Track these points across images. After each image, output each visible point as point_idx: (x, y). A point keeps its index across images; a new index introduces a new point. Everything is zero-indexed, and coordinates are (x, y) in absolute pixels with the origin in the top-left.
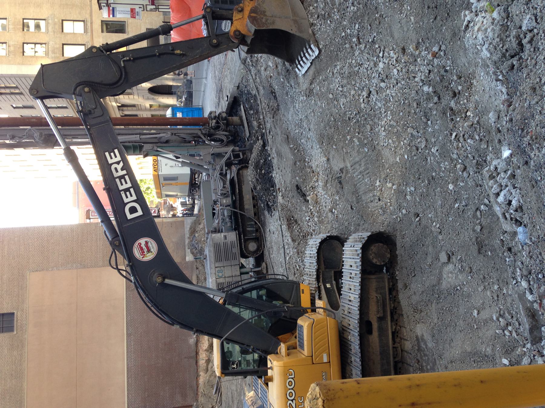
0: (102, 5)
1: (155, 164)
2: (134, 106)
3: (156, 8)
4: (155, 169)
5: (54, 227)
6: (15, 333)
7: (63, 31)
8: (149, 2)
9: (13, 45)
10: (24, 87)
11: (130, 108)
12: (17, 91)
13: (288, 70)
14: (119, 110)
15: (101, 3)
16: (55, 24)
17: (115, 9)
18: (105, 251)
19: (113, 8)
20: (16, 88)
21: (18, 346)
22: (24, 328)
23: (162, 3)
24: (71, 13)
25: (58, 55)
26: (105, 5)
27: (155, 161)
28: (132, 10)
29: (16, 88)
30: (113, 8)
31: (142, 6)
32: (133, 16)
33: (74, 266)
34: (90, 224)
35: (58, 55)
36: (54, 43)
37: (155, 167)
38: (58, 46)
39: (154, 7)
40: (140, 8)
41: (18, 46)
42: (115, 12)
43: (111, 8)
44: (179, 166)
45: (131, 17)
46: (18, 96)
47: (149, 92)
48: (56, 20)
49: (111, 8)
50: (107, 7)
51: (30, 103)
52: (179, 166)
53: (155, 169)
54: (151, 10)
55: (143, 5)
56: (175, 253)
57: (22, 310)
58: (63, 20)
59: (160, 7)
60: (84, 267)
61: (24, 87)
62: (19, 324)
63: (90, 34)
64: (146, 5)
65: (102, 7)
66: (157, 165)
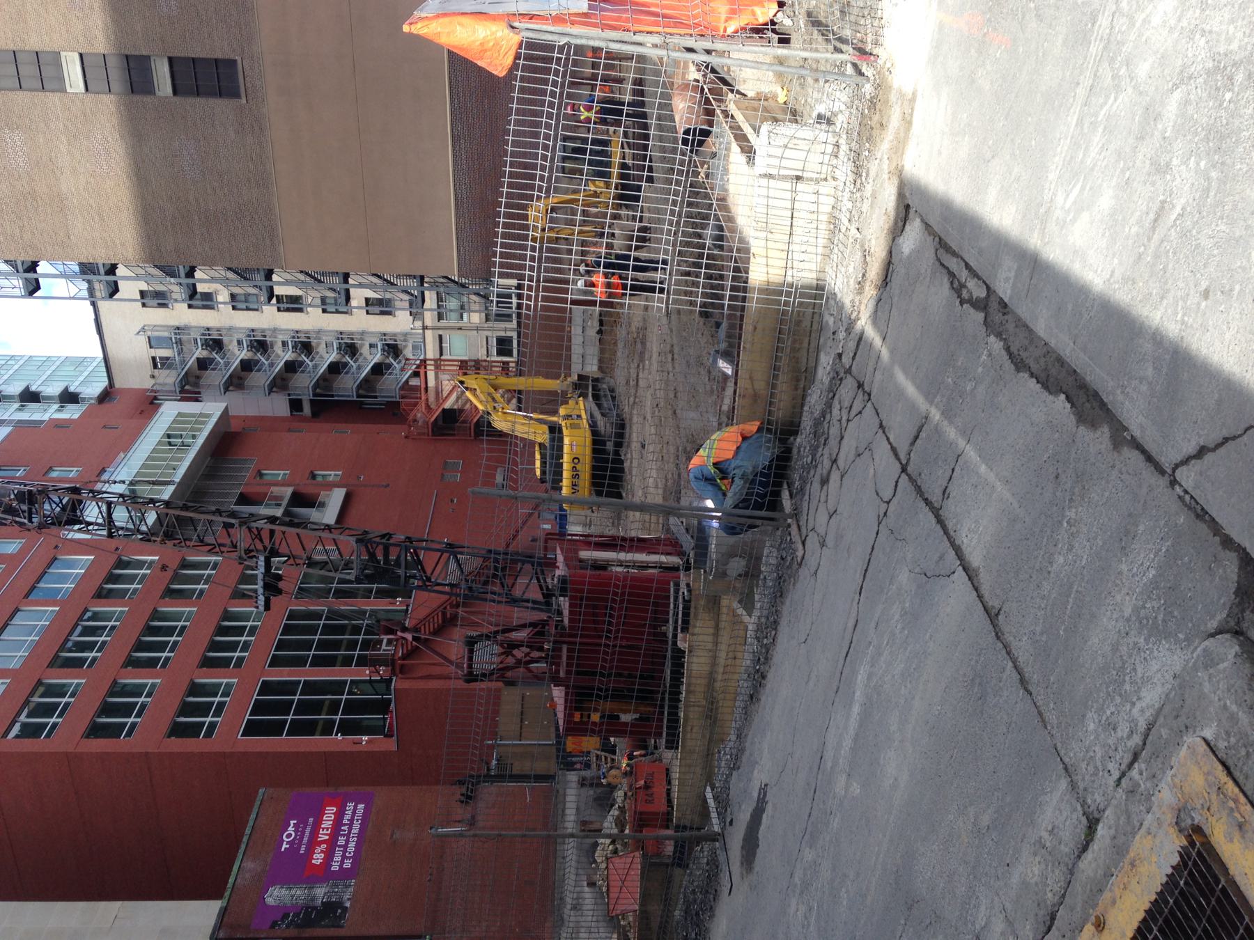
22: (259, 94)
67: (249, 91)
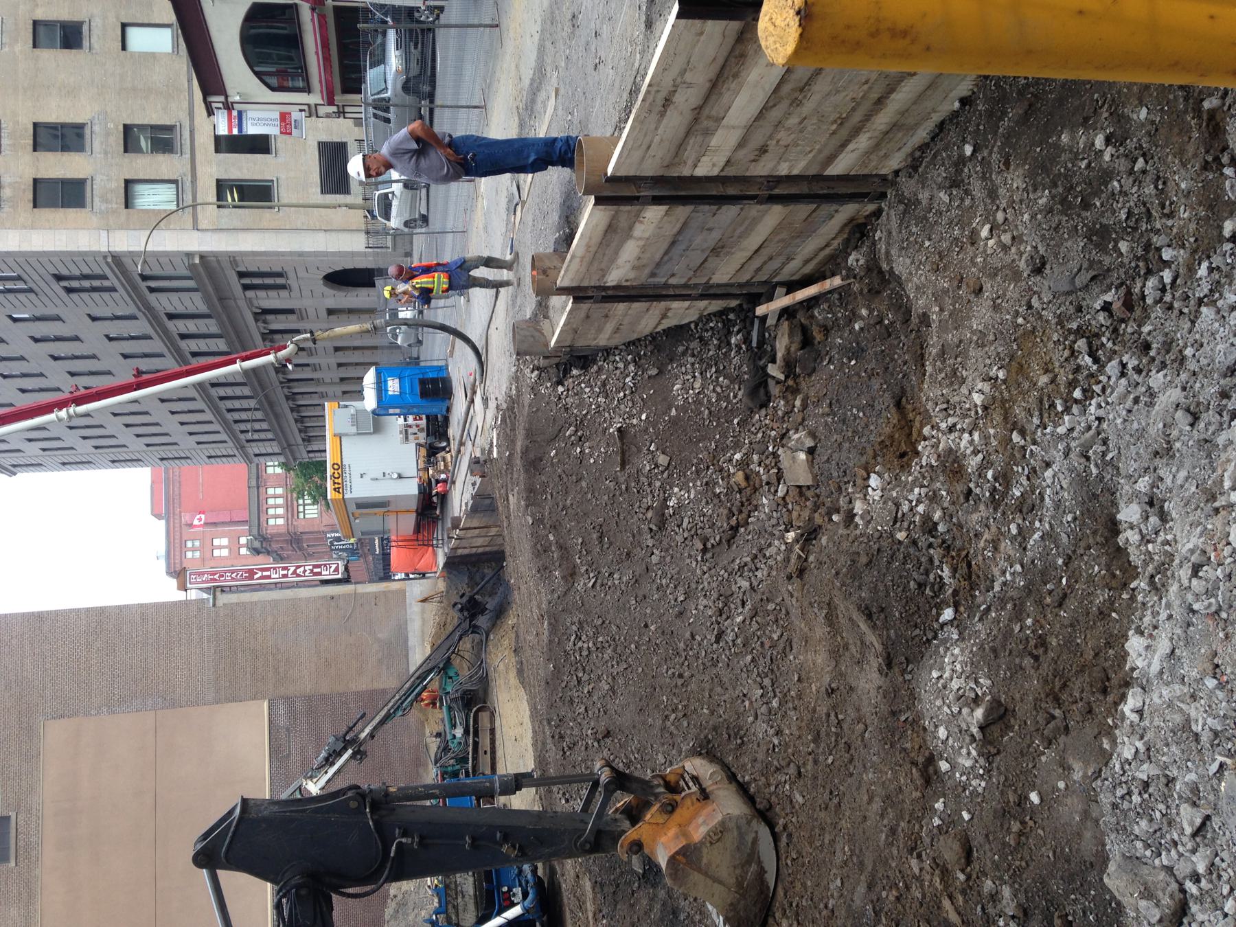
0: (214, 105)
1: (336, 475)
2: (291, 311)
3: (339, 112)
4: (337, 486)
5: (102, 611)
6: (13, 864)
7: (124, 48)
8: (323, 99)
9: (10, 184)
10: (36, 277)
11: (281, 317)
12: (20, 285)
13: (666, 100)
14: (257, 321)
15: (210, 102)
16: (108, 134)
17: (244, 115)
18: (221, 667)
19: (240, 113)
20: (19, 278)
21: (20, 894)
22: (33, 853)
23: (353, 101)
24: (144, 109)
25: (115, 206)
26: (220, 105)
27: (336, 467)
28: (284, 117)
29: (19, 278)
30: (240, 113)
31: (306, 108)
32: (286, 132)
33: (150, 702)
34: (187, 603)
35: (115, 206)
36: (105, 178)
37: (336, 481)
38: (113, 185)
39: (334, 109)
40: (301, 111)
41: (23, 187)
42: (244, 122)
43: (235, 113)
44: (392, 479)
45: (281, 133)
46: (21, 296)
47: (325, 285)
48: (110, 125)
49: (235, 113)
50: (226, 112)
51: (51, 311)
52: (392, 479)
53: (337, 486)
54: (328, 116)
55: (309, 105)
56: (384, 667)
57: (29, 811)
58: (124, 26)
59: (347, 109)
60: (173, 704)
61: (36, 277)
62: (21, 843)
63: (188, 156)
64: (316, 105)
65: (215, 111)
66: (341, 476)
67: (21, 851)
